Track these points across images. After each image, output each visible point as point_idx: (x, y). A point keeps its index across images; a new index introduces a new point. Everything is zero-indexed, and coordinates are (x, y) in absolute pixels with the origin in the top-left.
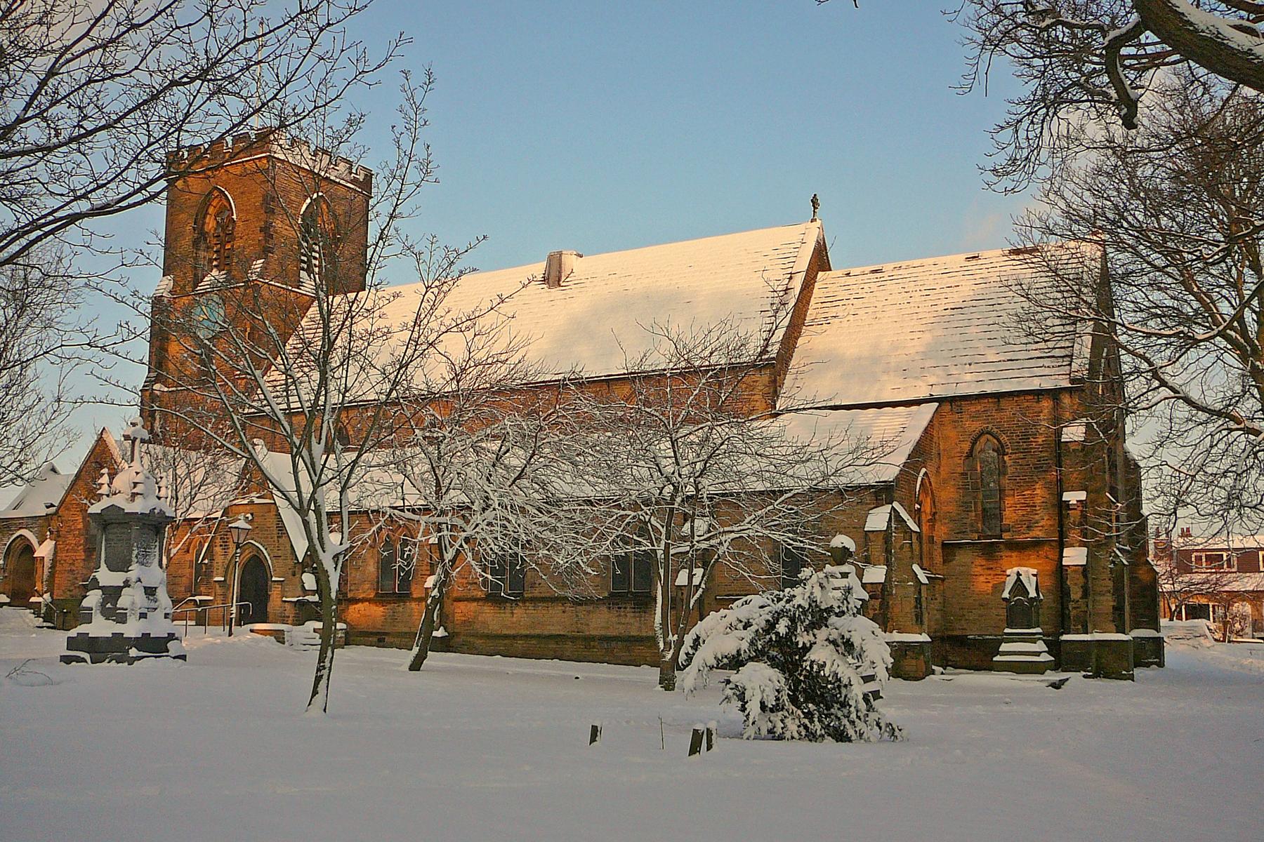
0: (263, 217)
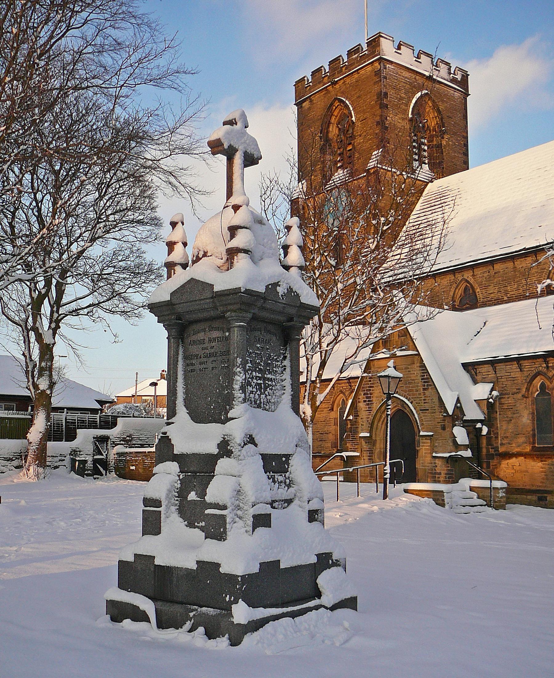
0: (379, 112)
